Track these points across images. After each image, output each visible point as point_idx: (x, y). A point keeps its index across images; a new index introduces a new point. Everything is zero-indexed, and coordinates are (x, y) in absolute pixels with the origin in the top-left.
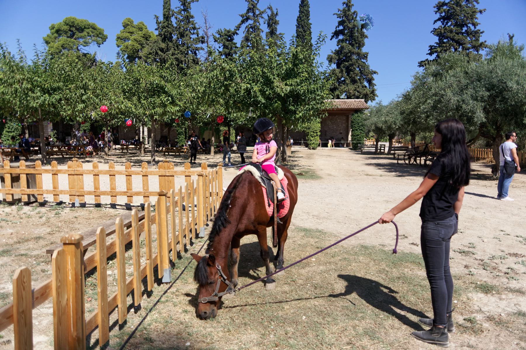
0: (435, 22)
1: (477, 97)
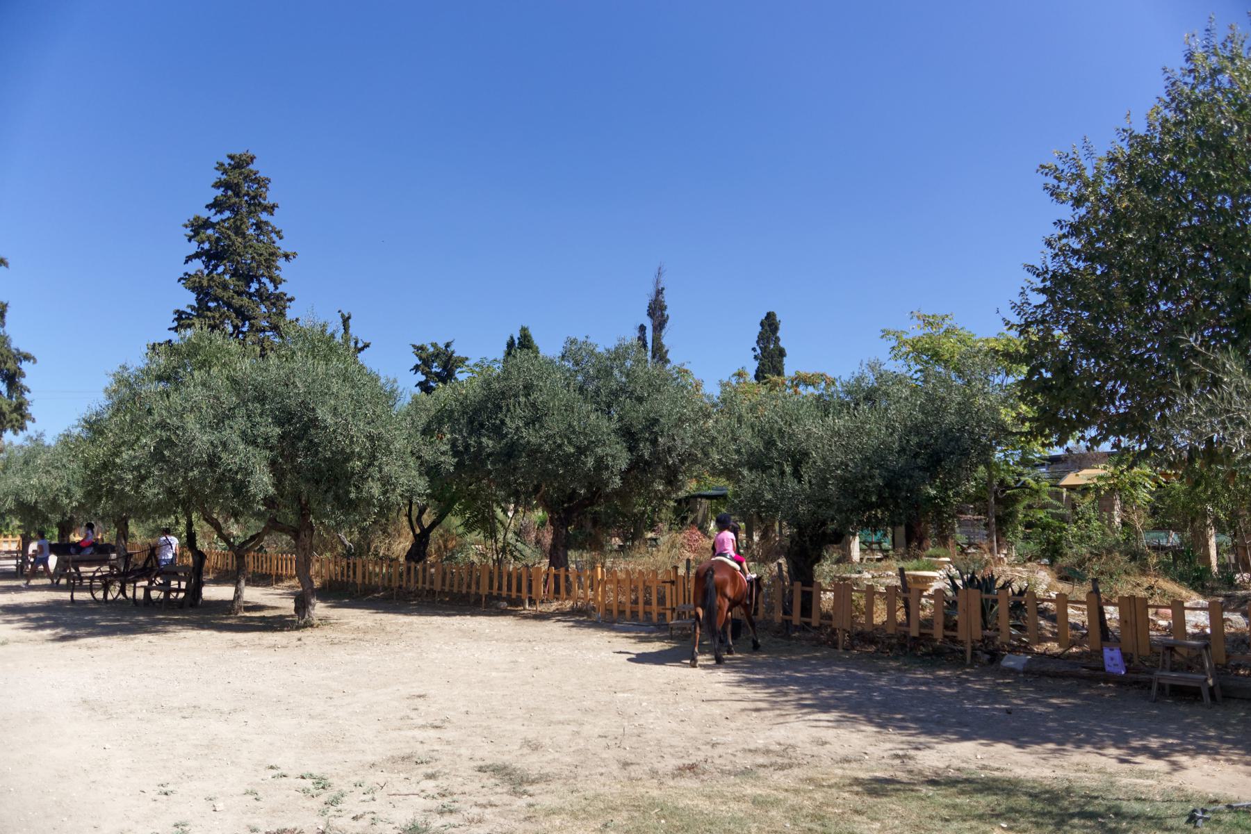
0: (189, 259)
1: (256, 437)
